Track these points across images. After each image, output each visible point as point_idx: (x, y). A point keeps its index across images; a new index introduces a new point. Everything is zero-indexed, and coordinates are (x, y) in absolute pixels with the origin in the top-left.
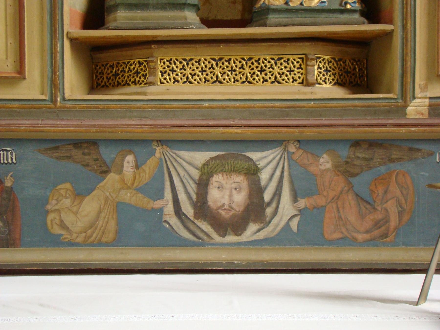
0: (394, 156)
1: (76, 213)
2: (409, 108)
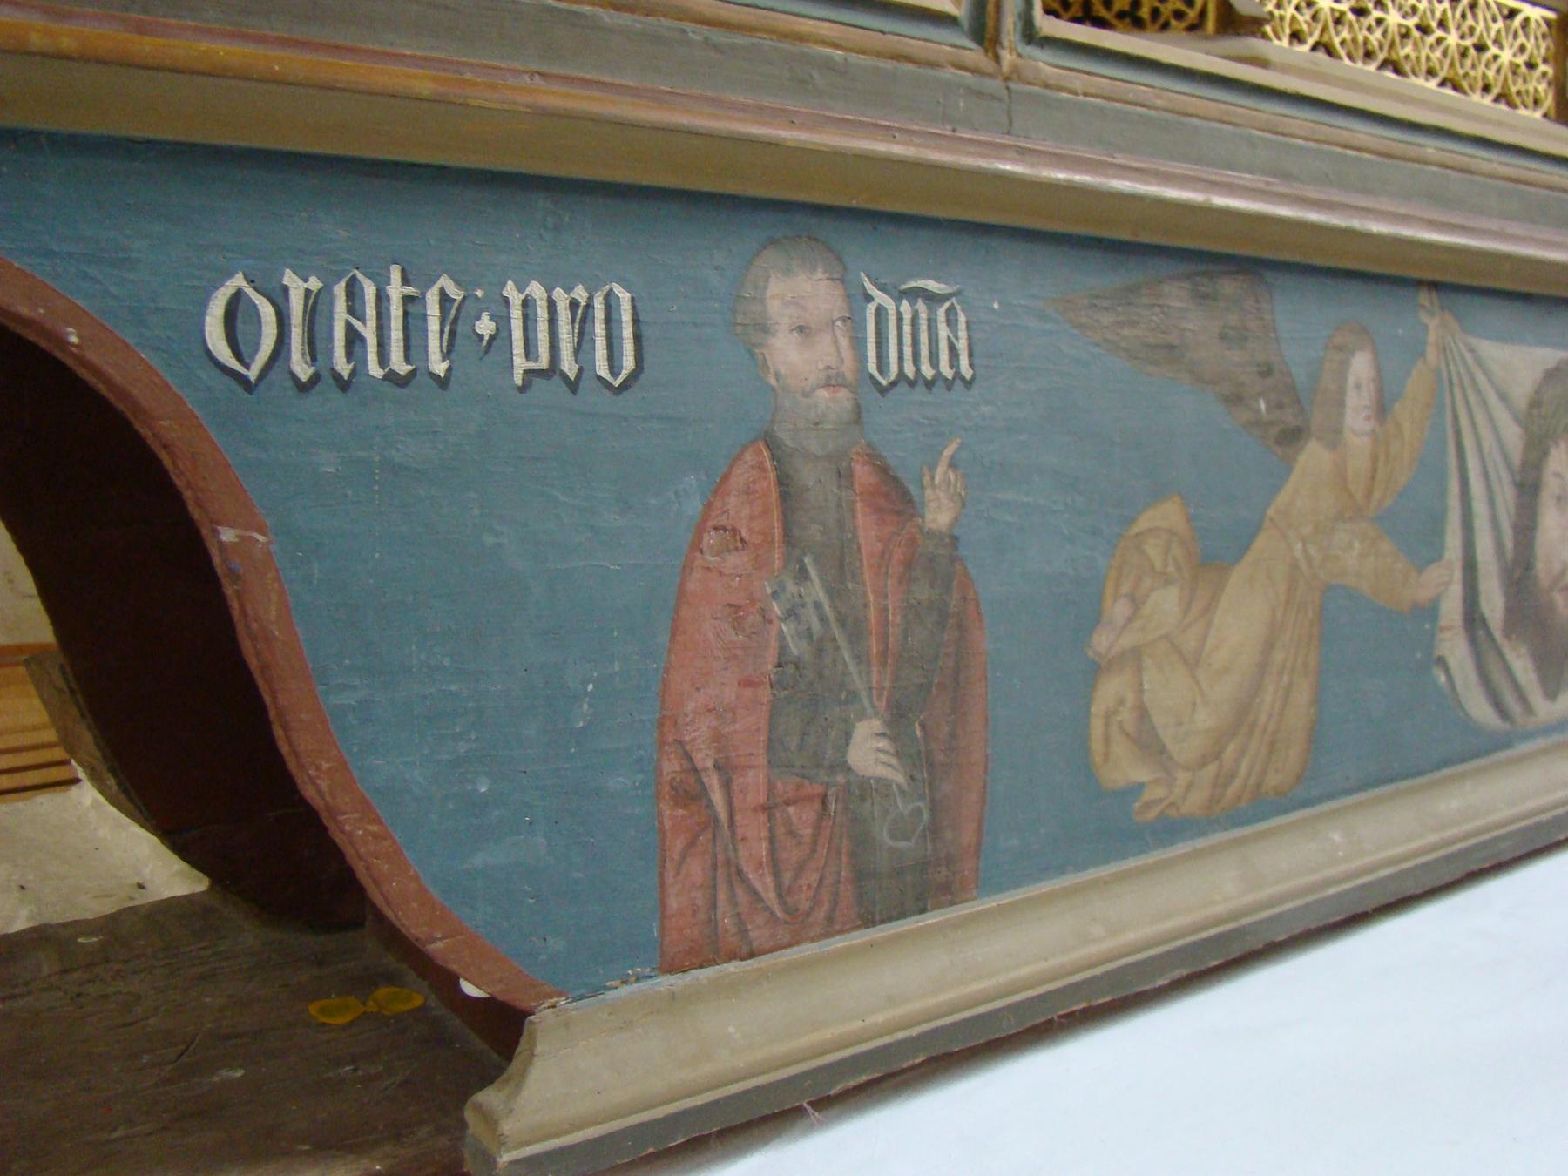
1: (1192, 662)
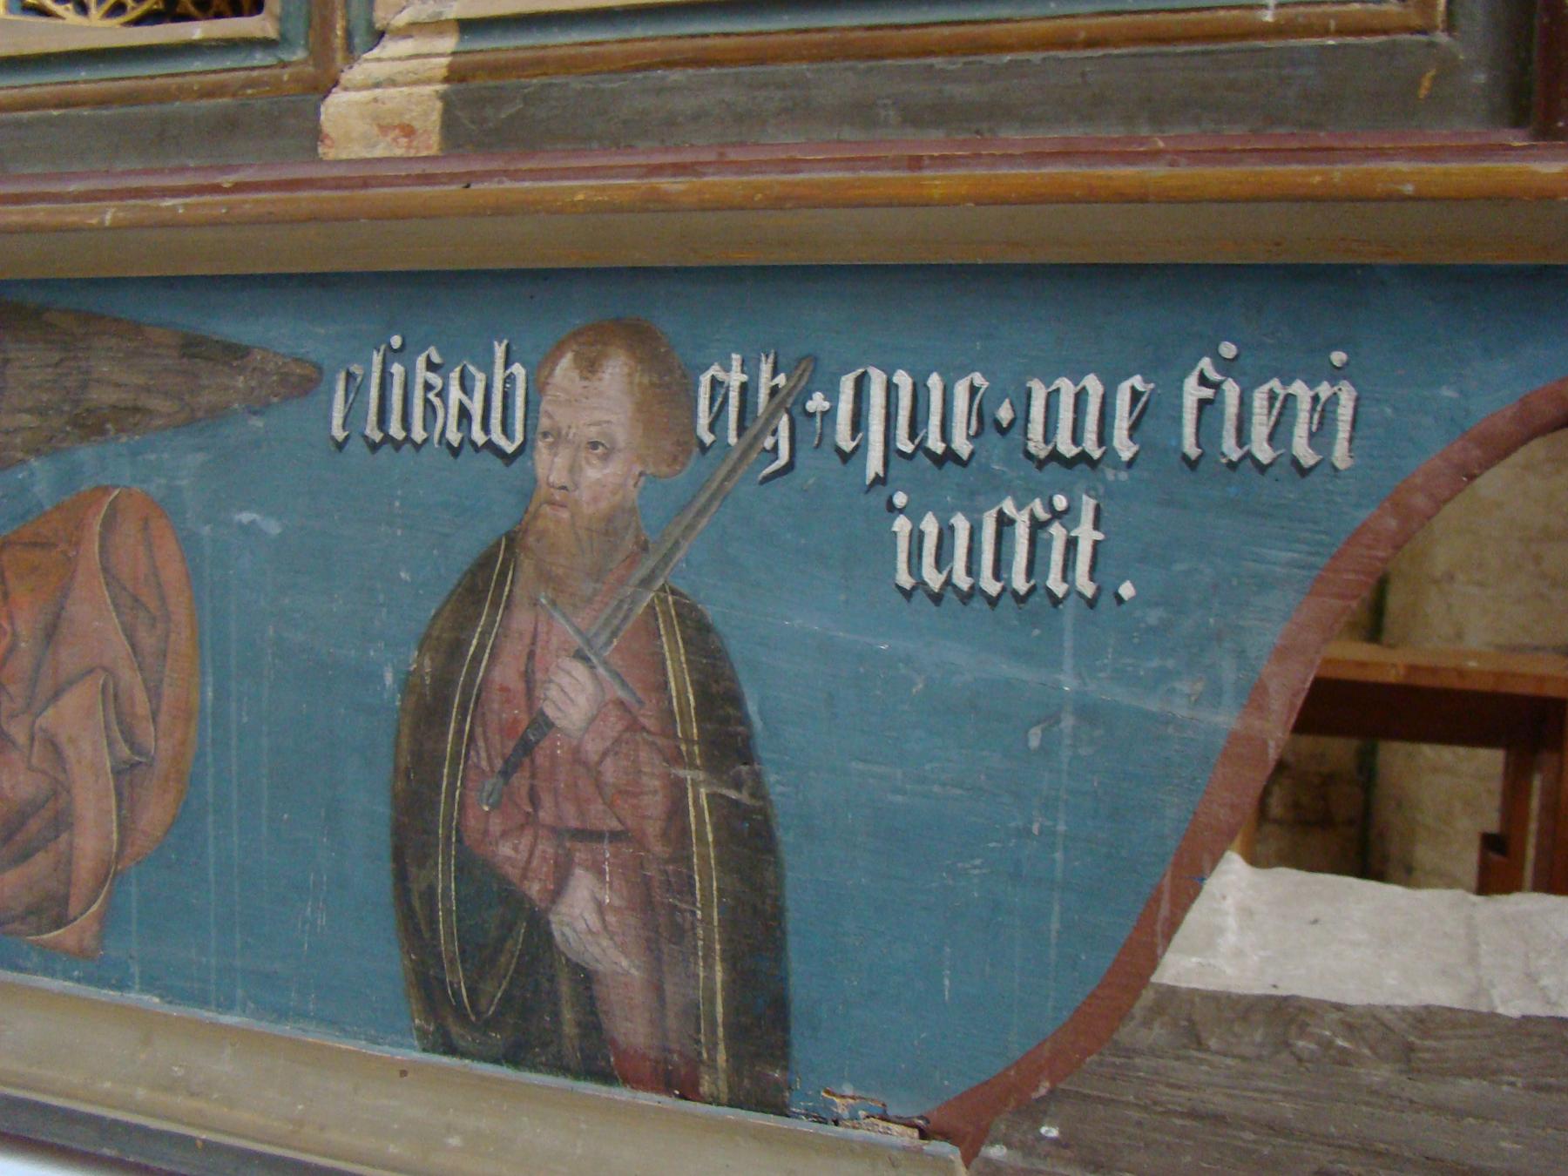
0: (102, 396)
2: (337, 99)
